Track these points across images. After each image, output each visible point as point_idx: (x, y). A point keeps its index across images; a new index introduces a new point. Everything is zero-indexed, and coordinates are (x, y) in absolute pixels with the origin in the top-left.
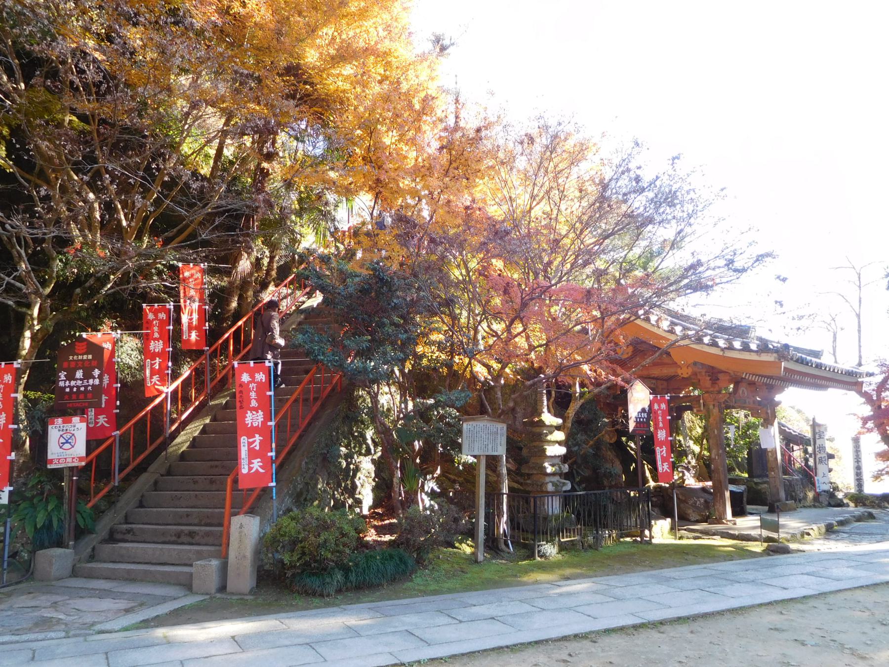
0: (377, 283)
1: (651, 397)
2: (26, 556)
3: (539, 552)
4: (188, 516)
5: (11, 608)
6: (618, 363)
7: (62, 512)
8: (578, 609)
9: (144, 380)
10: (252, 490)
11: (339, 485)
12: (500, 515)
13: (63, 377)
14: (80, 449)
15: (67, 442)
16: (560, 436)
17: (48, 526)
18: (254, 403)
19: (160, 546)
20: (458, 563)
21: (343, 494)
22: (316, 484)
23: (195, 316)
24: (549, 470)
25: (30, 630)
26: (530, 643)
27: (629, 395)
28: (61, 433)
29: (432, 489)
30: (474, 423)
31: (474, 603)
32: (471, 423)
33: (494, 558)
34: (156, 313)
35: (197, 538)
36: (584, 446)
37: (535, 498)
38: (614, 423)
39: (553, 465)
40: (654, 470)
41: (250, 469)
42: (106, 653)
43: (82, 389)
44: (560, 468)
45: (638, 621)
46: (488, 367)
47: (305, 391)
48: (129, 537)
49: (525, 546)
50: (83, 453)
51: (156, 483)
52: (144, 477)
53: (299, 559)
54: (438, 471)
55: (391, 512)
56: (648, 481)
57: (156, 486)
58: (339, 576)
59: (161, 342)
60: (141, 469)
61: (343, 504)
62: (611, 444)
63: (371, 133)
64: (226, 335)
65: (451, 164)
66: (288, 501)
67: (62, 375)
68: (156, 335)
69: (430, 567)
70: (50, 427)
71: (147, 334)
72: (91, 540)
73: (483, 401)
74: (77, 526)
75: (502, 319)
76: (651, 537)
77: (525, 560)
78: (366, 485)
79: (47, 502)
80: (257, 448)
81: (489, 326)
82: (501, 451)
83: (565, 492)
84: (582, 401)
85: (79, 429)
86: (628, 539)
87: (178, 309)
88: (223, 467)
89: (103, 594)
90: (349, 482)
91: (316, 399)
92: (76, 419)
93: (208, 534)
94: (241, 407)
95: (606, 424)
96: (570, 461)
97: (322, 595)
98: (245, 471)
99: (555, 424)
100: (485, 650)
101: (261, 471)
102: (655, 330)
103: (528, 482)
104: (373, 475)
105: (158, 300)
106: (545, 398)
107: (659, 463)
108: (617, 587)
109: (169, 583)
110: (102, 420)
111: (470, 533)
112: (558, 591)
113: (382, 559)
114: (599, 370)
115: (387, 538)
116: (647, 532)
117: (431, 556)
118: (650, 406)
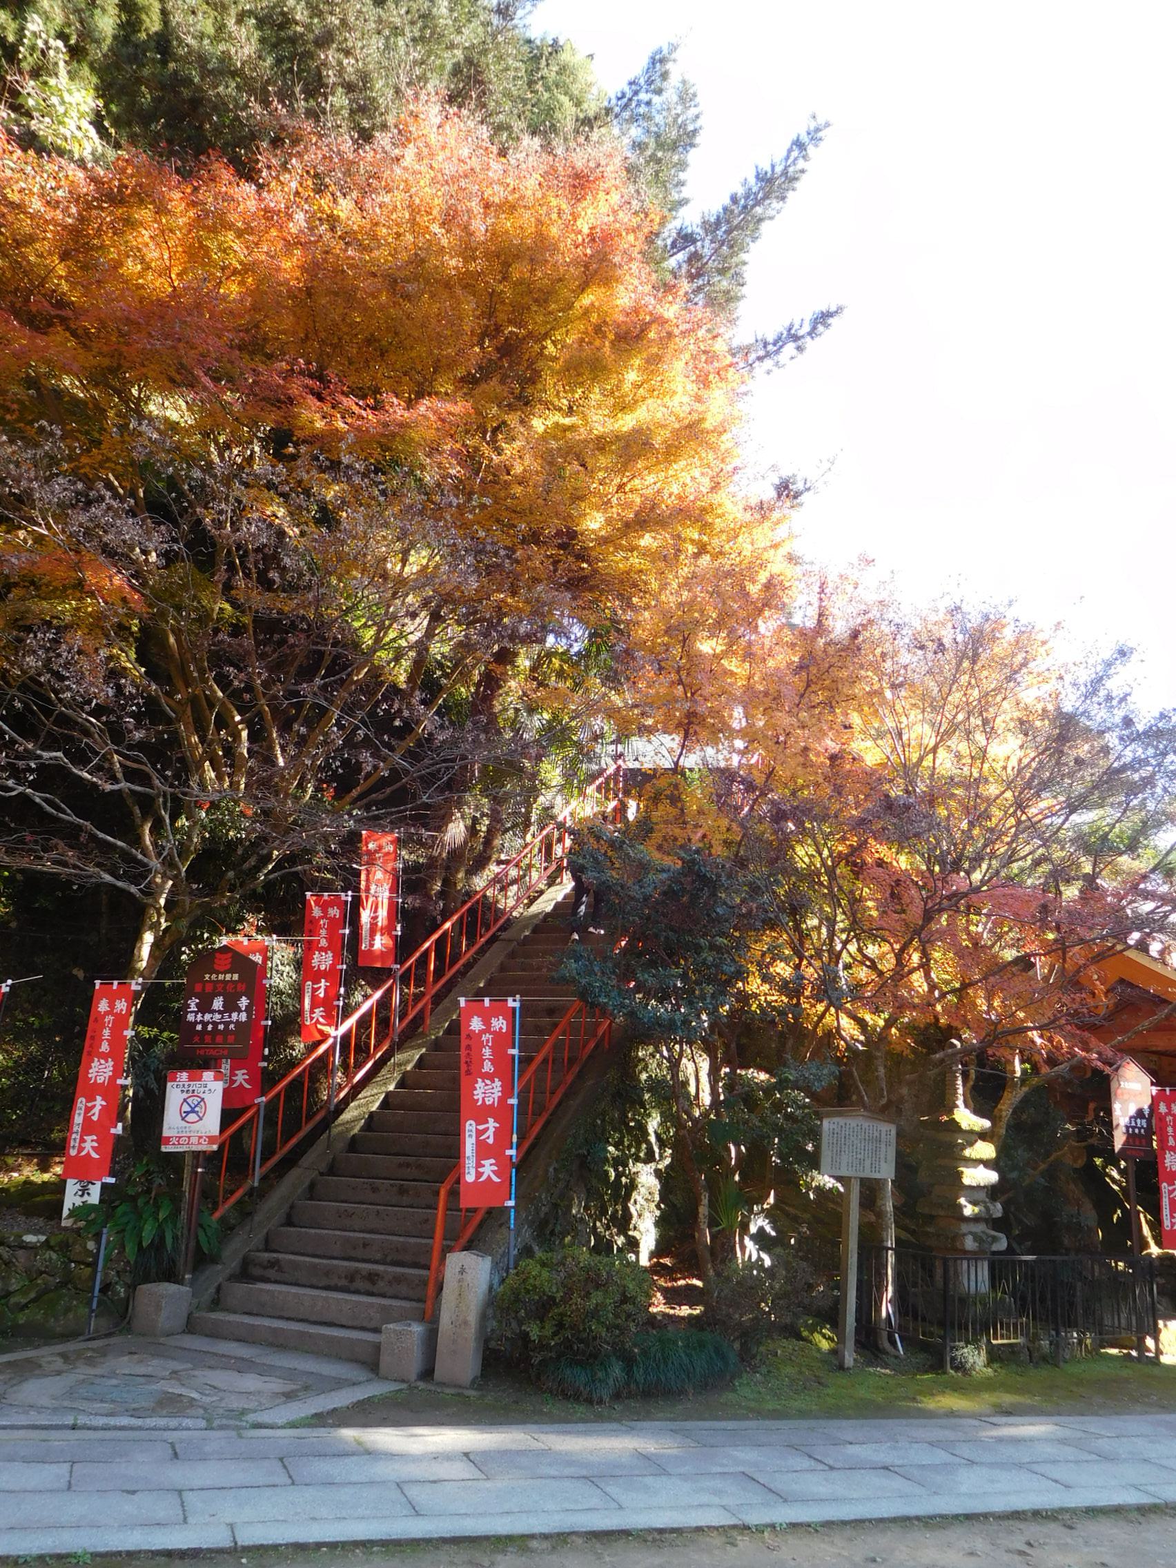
0: (693, 882)
1: (1154, 1090)
2: (122, 1291)
3: (953, 1359)
4: (365, 1245)
5: (113, 1374)
6: (1088, 1026)
7: (179, 1225)
8: (1035, 1467)
9: (300, 1013)
10: (475, 1210)
11: (604, 1212)
12: (881, 1289)
13: (193, 1007)
14: (211, 1123)
15: (193, 1111)
16: (985, 1150)
17: (158, 1244)
18: (488, 1067)
19: (324, 1294)
20: (809, 1368)
21: (608, 1228)
22: (570, 1207)
23: (383, 913)
24: (969, 1210)
25: (152, 1412)
26: (956, 1517)
27: (1114, 1085)
28: (185, 1095)
29: (761, 1229)
30: (840, 1121)
31: (850, 1438)
32: (836, 1120)
33: (870, 1364)
34: (324, 907)
35: (381, 1284)
36: (1030, 1171)
37: (945, 1262)
38: (1081, 1135)
39: (974, 1203)
40: (1156, 1225)
41: (479, 1175)
42: (281, 1459)
43: (221, 1027)
44: (987, 1209)
45: (1145, 1500)
46: (861, 1023)
47: (557, 1046)
48: (271, 1273)
49: (925, 1347)
50: (215, 1130)
51: (312, 1186)
52: (294, 1174)
53: (555, 1334)
54: (771, 1200)
55: (690, 1265)
56: (1145, 1245)
57: (312, 1192)
58: (617, 1370)
59: (330, 954)
60: (290, 1162)
61: (610, 1243)
62: (1075, 1170)
63: (685, 640)
64: (427, 945)
65: (808, 686)
66: (527, 1233)
67: (193, 1004)
68: (324, 943)
69: (764, 1369)
70: (169, 1084)
71: (309, 942)
72: (218, 1274)
73: (850, 1081)
74: (198, 1247)
75: (884, 940)
76: (1159, 1352)
77: (926, 1372)
78: (647, 1214)
79: (157, 1207)
80: (491, 1141)
81: (860, 950)
82: (886, 1172)
83: (994, 1253)
84: (1025, 1089)
85: (212, 1089)
86: (1114, 1351)
87: (357, 903)
88: (419, 1166)
89: (244, 1366)
90: (619, 1207)
91: (572, 1061)
92: (208, 1075)
93: (398, 1279)
94: (468, 1073)
95: (1067, 1135)
96: (1004, 1198)
97: (589, 1401)
98: (470, 1178)
99: (977, 1129)
100: (882, 1520)
101: (496, 1179)
102: (1158, 968)
103: (930, 1230)
104: (657, 1198)
105: (327, 886)
106: (959, 1082)
107: (1166, 1212)
108: (1102, 1437)
109: (339, 1358)
110: (241, 1077)
111: (831, 1316)
112: (996, 1433)
113: (687, 1346)
114: (1058, 1038)
115: (685, 1311)
116: (1150, 1342)
117: (762, 1349)
118: (1153, 1107)
